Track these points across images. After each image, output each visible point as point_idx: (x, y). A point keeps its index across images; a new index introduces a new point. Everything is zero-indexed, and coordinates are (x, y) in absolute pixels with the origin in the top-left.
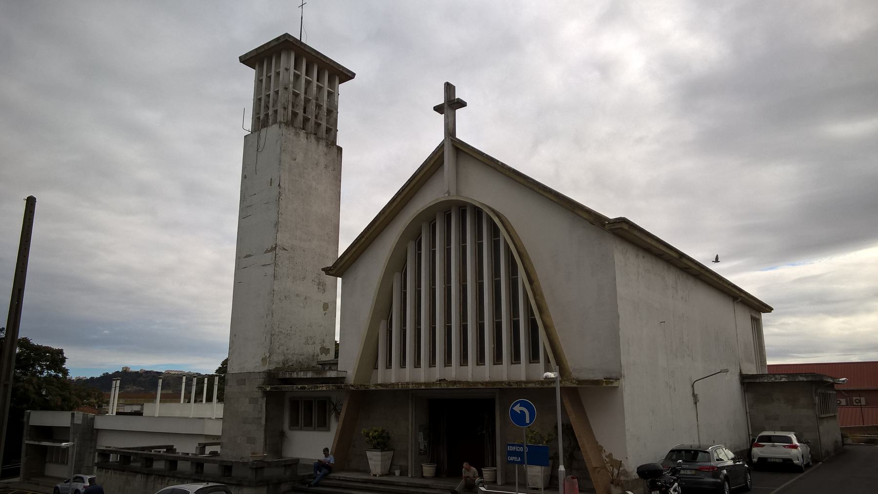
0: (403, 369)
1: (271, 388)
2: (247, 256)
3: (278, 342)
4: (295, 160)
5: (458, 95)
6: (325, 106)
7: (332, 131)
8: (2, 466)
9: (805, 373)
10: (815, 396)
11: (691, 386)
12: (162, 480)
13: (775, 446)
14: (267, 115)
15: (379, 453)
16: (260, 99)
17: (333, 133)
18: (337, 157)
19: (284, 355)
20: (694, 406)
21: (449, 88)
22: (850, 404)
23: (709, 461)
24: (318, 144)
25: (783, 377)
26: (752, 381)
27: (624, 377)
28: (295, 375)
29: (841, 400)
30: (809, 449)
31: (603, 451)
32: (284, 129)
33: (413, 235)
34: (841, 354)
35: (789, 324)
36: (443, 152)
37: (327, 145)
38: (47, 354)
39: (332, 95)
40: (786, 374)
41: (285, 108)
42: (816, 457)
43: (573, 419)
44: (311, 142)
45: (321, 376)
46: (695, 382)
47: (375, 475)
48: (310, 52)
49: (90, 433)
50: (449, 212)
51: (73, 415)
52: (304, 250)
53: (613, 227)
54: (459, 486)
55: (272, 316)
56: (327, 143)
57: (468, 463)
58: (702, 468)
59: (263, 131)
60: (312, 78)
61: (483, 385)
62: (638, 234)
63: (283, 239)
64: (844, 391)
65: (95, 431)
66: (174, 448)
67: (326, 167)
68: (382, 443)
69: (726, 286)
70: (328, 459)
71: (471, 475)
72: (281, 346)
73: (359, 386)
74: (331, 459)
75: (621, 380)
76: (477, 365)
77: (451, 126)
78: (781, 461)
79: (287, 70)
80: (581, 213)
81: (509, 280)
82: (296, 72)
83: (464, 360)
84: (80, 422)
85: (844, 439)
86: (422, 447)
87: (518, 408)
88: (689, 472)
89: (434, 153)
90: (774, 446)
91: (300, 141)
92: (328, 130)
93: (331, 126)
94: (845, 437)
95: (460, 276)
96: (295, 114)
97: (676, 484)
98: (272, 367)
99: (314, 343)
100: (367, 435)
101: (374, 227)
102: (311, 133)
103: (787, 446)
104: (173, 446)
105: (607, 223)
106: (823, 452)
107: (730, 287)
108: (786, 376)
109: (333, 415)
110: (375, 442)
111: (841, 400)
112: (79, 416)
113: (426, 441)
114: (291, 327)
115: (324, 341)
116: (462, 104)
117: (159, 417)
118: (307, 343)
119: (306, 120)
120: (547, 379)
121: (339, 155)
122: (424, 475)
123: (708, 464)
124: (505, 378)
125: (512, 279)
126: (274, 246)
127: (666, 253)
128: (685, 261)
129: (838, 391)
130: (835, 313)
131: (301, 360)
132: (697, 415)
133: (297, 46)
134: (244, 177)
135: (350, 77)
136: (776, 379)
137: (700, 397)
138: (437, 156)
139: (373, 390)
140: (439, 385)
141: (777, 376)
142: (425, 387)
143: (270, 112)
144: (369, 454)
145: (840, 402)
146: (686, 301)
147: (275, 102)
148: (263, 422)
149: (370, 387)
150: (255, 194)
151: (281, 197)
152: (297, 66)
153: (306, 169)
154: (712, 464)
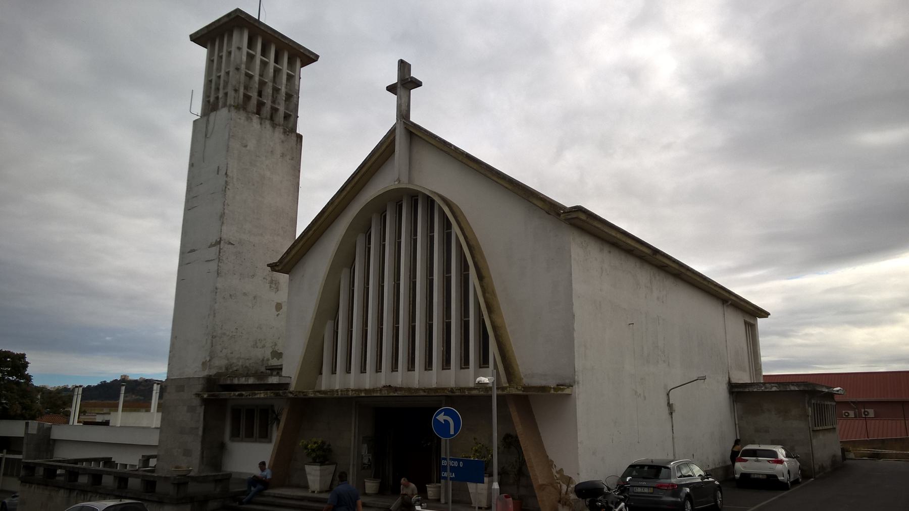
0: (348, 374)
1: (209, 396)
2: (193, 251)
3: (220, 344)
4: (246, 146)
5: (414, 74)
6: (283, 90)
7: (291, 117)
8: (155, 470)
9: (804, 382)
10: (808, 407)
11: (666, 394)
12: (84, 495)
13: (760, 461)
14: (217, 98)
15: (318, 468)
16: (211, 81)
17: (292, 119)
18: (296, 145)
19: (228, 360)
20: (670, 417)
21: (403, 66)
22: (858, 416)
23: (669, 477)
24: (274, 132)
25: (774, 386)
26: (741, 390)
27: (578, 383)
28: (236, 381)
29: (849, 412)
30: (798, 464)
31: (554, 466)
32: (234, 113)
33: (362, 227)
34: (865, 365)
35: (812, 335)
36: (395, 137)
37: (285, 132)
38: (8, 359)
39: (292, 79)
40: (777, 383)
41: (236, 91)
42: (807, 473)
43: (520, 430)
44: (265, 128)
45: (262, 382)
46: (672, 389)
47: (314, 492)
48: (266, 30)
49: (47, 443)
50: (400, 203)
51: (27, 424)
52: (254, 245)
53: (569, 217)
54: (395, 503)
55: (214, 316)
56: (284, 129)
57: (406, 480)
58: (661, 486)
59: (213, 115)
60: (269, 59)
61: (425, 392)
62: (599, 226)
63: (229, 232)
64: (852, 402)
65: (51, 442)
66: (113, 460)
67: (283, 155)
68: (323, 456)
69: (713, 287)
70: (265, 473)
71: (410, 493)
72: (224, 350)
73: (297, 393)
74: (268, 474)
75: (574, 387)
76: (408, 371)
77: (404, 107)
78: (765, 477)
79: (239, 49)
80: (535, 202)
81: (461, 276)
82: (251, 51)
83: (411, 366)
84: (35, 432)
85: (846, 453)
86: (366, 461)
87: (441, 418)
88: (646, 490)
89: (386, 137)
90: (758, 461)
91: (253, 126)
92: (287, 117)
93: (291, 112)
94: (847, 451)
95: (410, 273)
96: (247, 98)
97: (623, 504)
98: (213, 372)
99: (264, 347)
100: (306, 447)
101: (322, 219)
102: (266, 119)
103: (771, 461)
104: (111, 458)
105: (562, 212)
106: (817, 467)
107: (717, 289)
108: (776, 385)
109: (275, 424)
110: (314, 455)
111: (849, 412)
112: (34, 426)
113: (370, 455)
114: (237, 329)
115: (276, 345)
116: (417, 84)
117: (120, 427)
118: (255, 346)
119: (260, 105)
120: (480, 385)
121: (299, 143)
122: (367, 492)
123: (668, 481)
124: (452, 384)
125: (464, 274)
126: (218, 240)
127: (637, 248)
128: (661, 258)
129: (838, 403)
130: (859, 324)
131: (248, 365)
132: (673, 427)
133: (250, 23)
134: (191, 165)
135: (314, 60)
136: (766, 388)
137: (677, 407)
138: (389, 141)
139: (312, 398)
140: (379, 391)
141: (768, 385)
142: (366, 394)
143: (221, 95)
144: (308, 469)
145: (848, 413)
146: (663, 302)
147: (226, 83)
148: (200, 433)
149: (309, 394)
150: (202, 184)
151: (228, 187)
152: (251, 45)
153: (259, 156)
154: (673, 481)
